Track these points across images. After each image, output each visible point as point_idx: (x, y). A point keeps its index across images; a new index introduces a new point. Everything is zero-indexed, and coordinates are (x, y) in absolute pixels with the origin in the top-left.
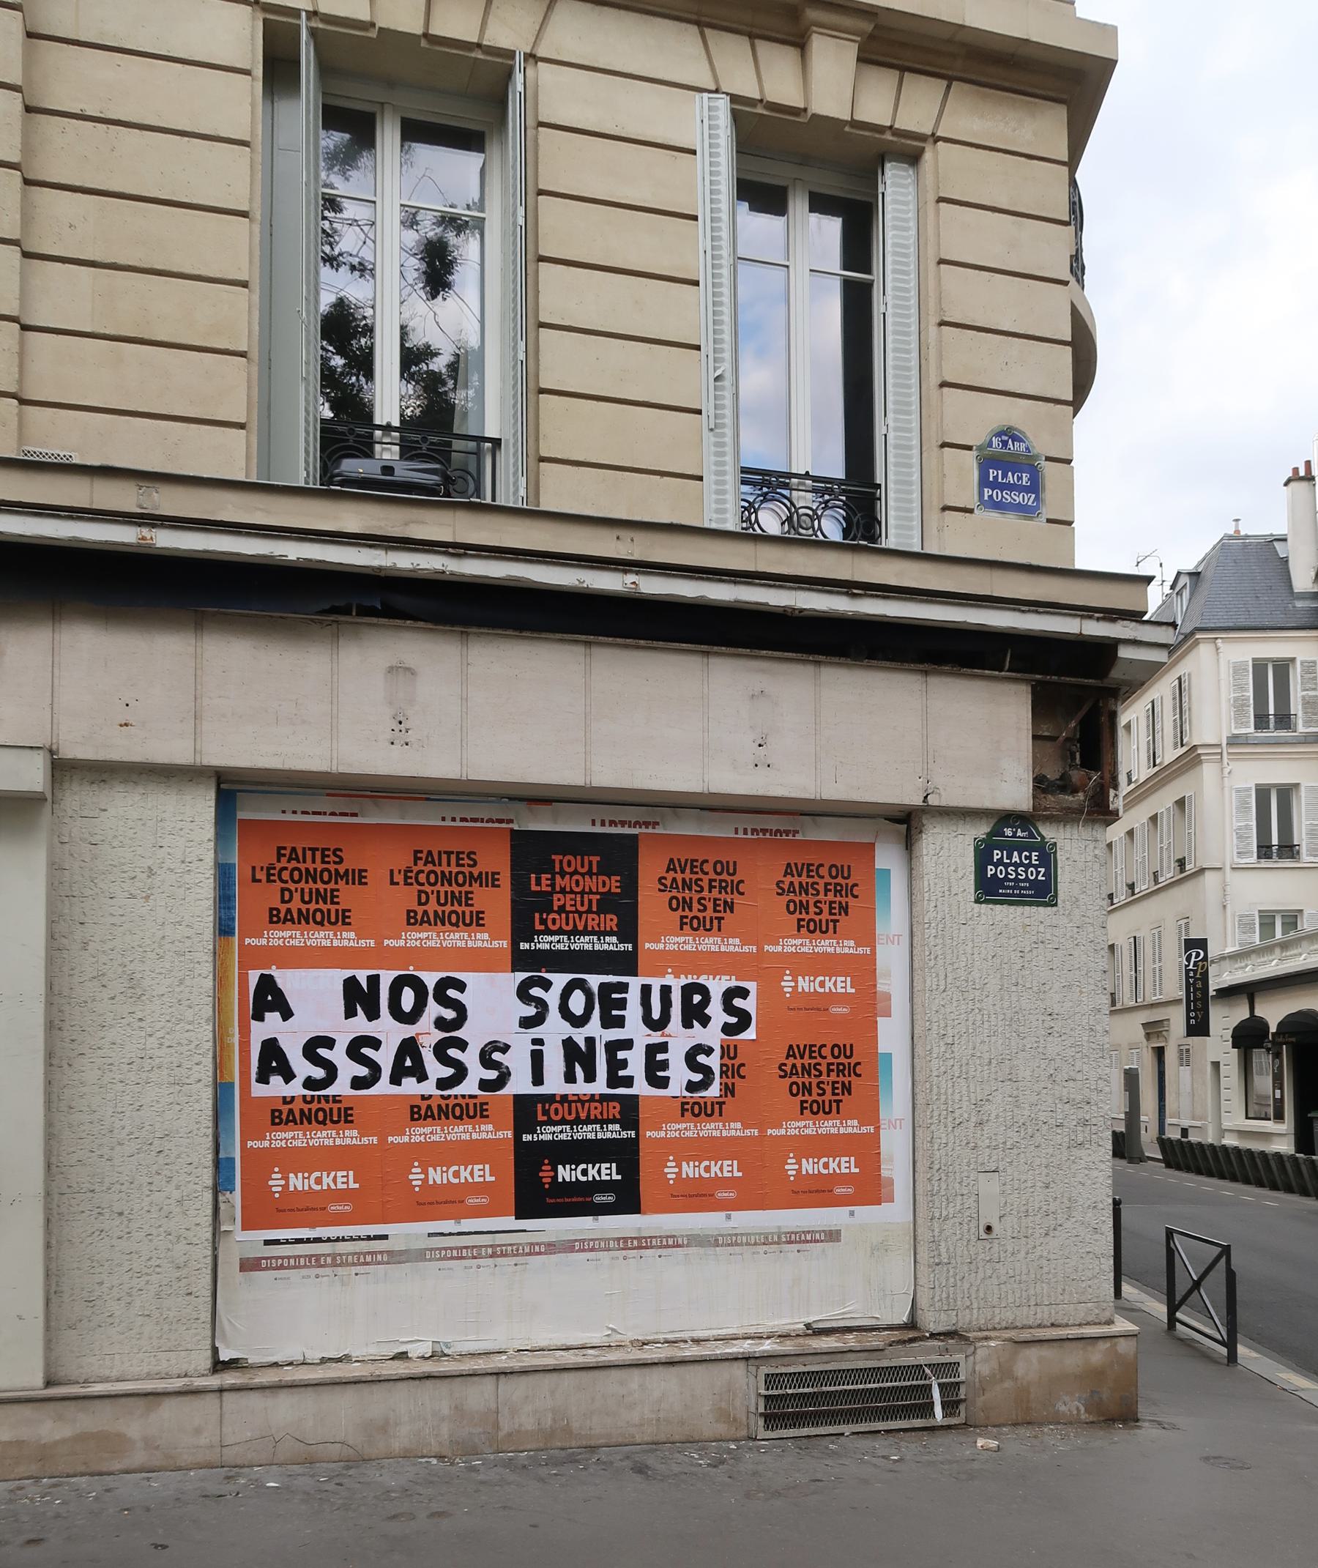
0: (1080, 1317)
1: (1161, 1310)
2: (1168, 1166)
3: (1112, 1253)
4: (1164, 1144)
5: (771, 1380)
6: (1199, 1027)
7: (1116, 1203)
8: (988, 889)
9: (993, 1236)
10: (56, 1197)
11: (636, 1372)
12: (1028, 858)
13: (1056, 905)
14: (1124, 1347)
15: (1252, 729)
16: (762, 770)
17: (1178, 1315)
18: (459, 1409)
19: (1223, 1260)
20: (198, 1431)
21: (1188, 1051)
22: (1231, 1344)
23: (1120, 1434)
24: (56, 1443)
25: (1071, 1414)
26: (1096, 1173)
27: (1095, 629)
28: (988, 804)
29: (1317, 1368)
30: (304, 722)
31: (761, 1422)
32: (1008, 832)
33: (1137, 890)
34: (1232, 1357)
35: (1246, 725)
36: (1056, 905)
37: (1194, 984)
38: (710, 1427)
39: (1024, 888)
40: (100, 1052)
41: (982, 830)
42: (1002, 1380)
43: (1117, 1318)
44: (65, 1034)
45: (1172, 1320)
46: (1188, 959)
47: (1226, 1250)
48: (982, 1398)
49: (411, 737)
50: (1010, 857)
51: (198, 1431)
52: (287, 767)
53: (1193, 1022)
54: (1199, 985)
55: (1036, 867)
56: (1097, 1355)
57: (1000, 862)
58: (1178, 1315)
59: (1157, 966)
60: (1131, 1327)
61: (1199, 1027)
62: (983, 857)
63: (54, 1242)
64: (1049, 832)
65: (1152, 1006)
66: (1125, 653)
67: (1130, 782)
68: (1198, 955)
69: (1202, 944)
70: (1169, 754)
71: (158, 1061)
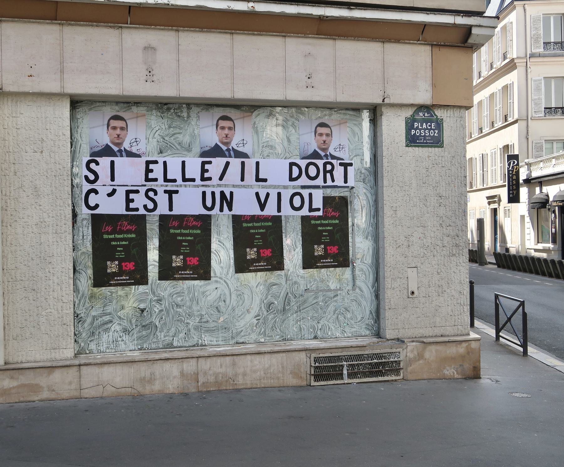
0: (452, 333)
1: (492, 332)
2: (499, 266)
3: (469, 303)
4: (496, 255)
5: (316, 360)
6: (514, 198)
7: (471, 283)
8: (412, 141)
9: (415, 296)
10: (6, 283)
11: (257, 356)
13: (443, 147)
14: (474, 345)
15: (542, 50)
16: (310, 89)
17: (501, 334)
18: (182, 374)
19: (521, 308)
20: (70, 383)
21: (509, 210)
22: (524, 346)
23: (471, 383)
24: (11, 389)
25: (450, 375)
26: (462, 270)
27: (460, 20)
28: (411, 102)
29: (563, 354)
30: (108, 73)
31: (313, 378)
32: (421, 114)
33: (483, 131)
34: (525, 352)
35: (539, 47)
36: (443, 147)
37: (512, 177)
38: (292, 381)
39: (428, 140)
40: (24, 220)
41: (409, 113)
42: (419, 360)
43: (471, 333)
44: (9, 212)
45: (498, 337)
46: (509, 165)
47: (522, 304)
48: (411, 368)
49: (155, 78)
50: (422, 126)
51: (70, 383)
52: (101, 93)
53: (511, 196)
54: (515, 177)
55: (434, 130)
56: (461, 349)
58: (501, 334)
59: (494, 168)
60: (477, 336)
61: (514, 198)
62: (410, 124)
63: (6, 303)
64: (439, 113)
65: (491, 188)
66: (474, 31)
67: (480, 77)
68: (514, 162)
69: (516, 157)
70: (498, 64)
71: (48, 223)
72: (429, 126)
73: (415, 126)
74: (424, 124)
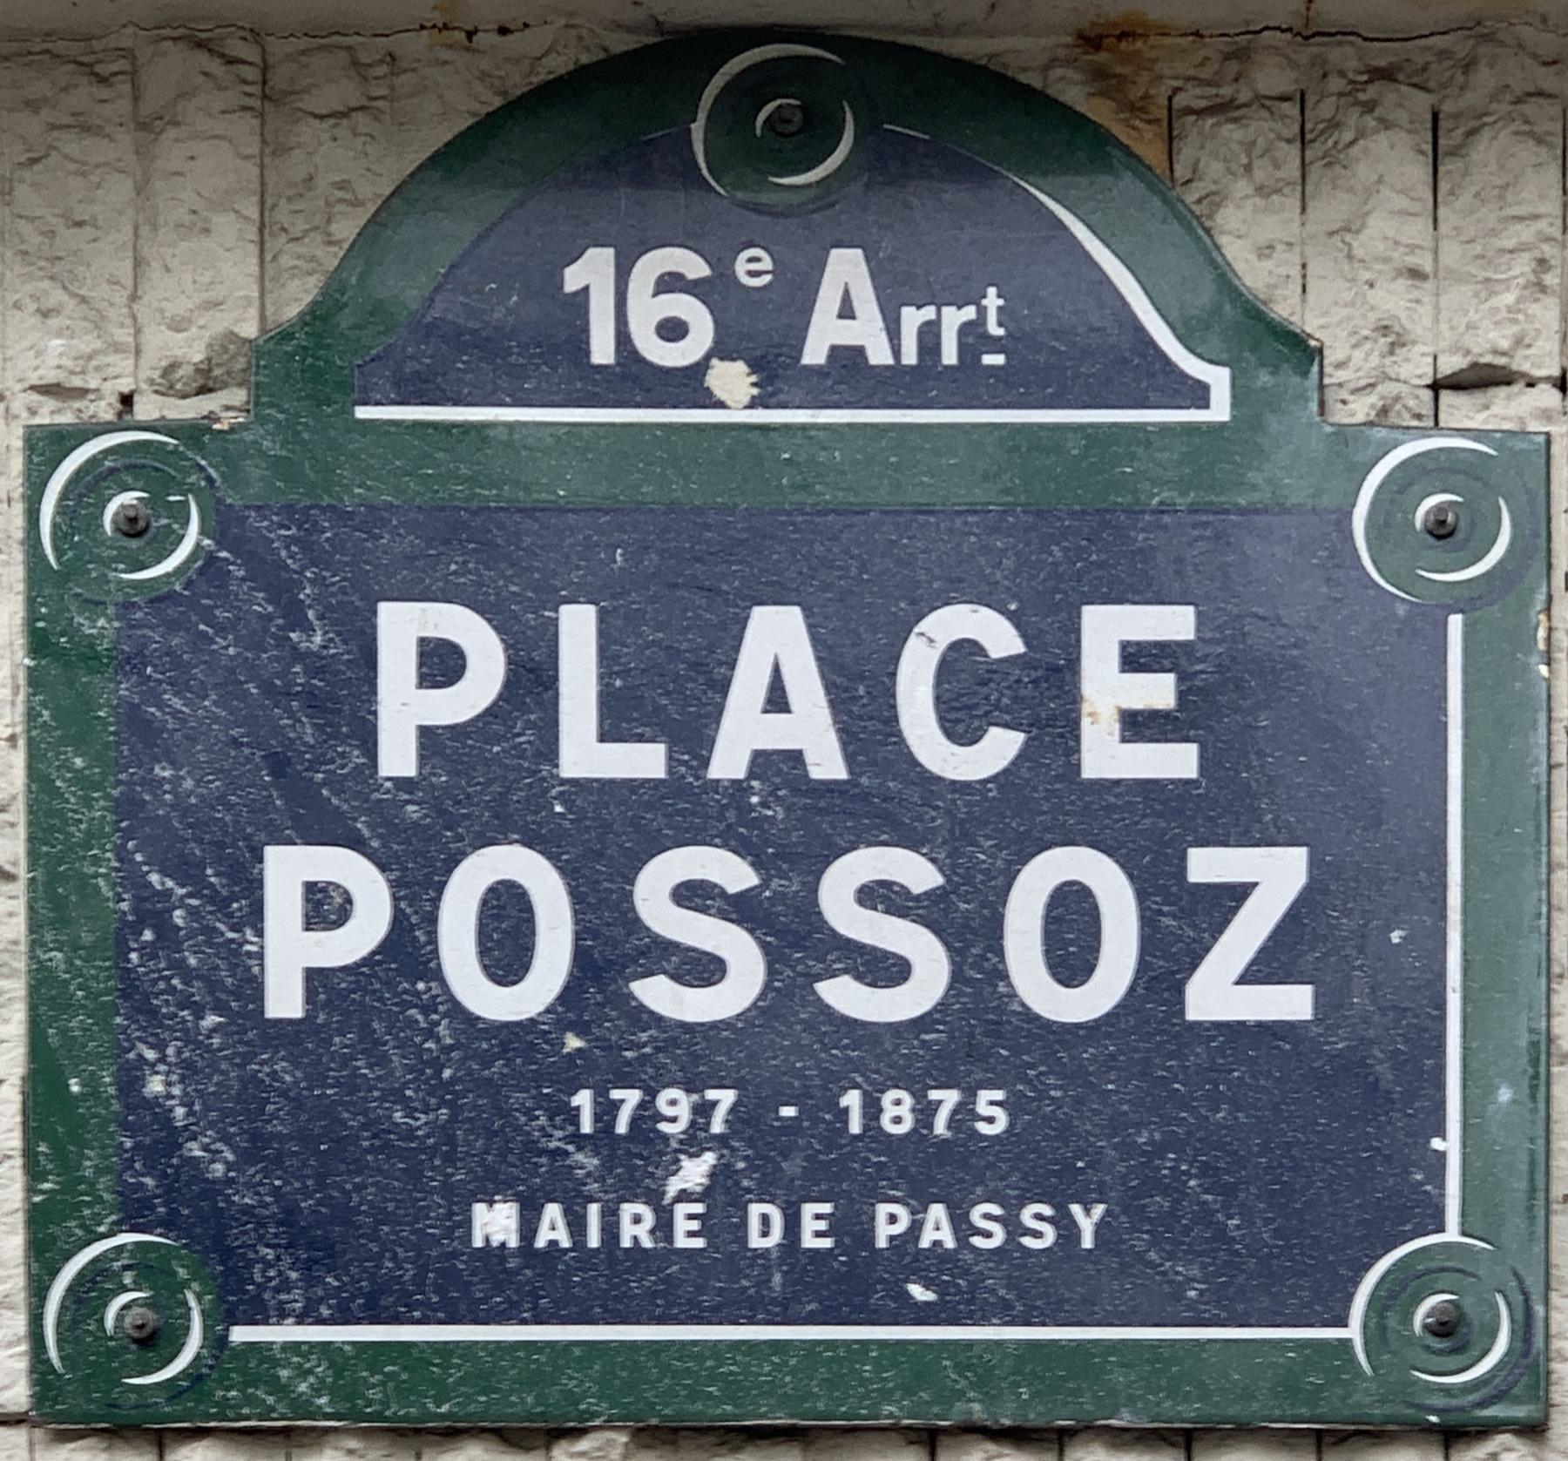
12: (1041, 692)
32: (638, 298)
39: (940, 1168)
50: (668, 689)
55: (1146, 829)
57: (494, 775)
72: (968, 694)
73: (404, 714)
74: (776, 637)
